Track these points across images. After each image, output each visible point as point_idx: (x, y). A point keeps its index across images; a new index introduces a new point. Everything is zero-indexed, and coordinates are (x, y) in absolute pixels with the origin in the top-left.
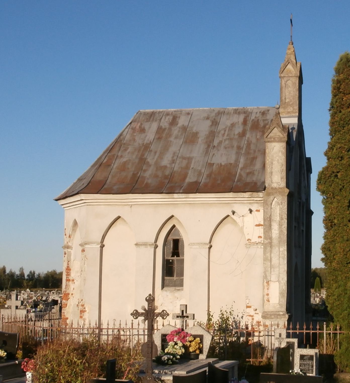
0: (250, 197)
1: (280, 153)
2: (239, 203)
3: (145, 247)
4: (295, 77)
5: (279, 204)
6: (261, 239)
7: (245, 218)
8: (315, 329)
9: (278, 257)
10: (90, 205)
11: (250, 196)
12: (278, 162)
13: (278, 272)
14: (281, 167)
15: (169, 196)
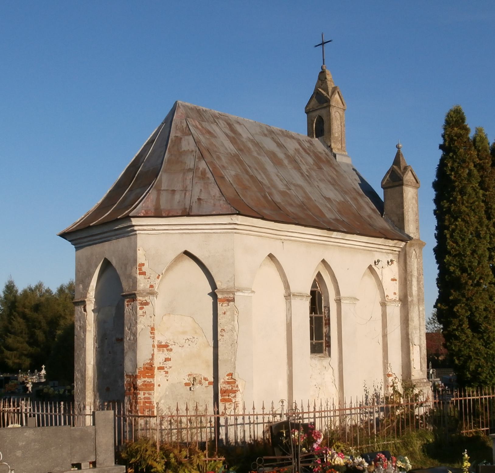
0: (391, 246)
2: (379, 252)
3: (301, 300)
4: (342, 110)
6: (396, 296)
7: (384, 270)
8: (461, 396)
10: (238, 233)
11: (393, 245)
12: (413, 210)
13: (419, 334)
14: (415, 216)
15: (328, 234)
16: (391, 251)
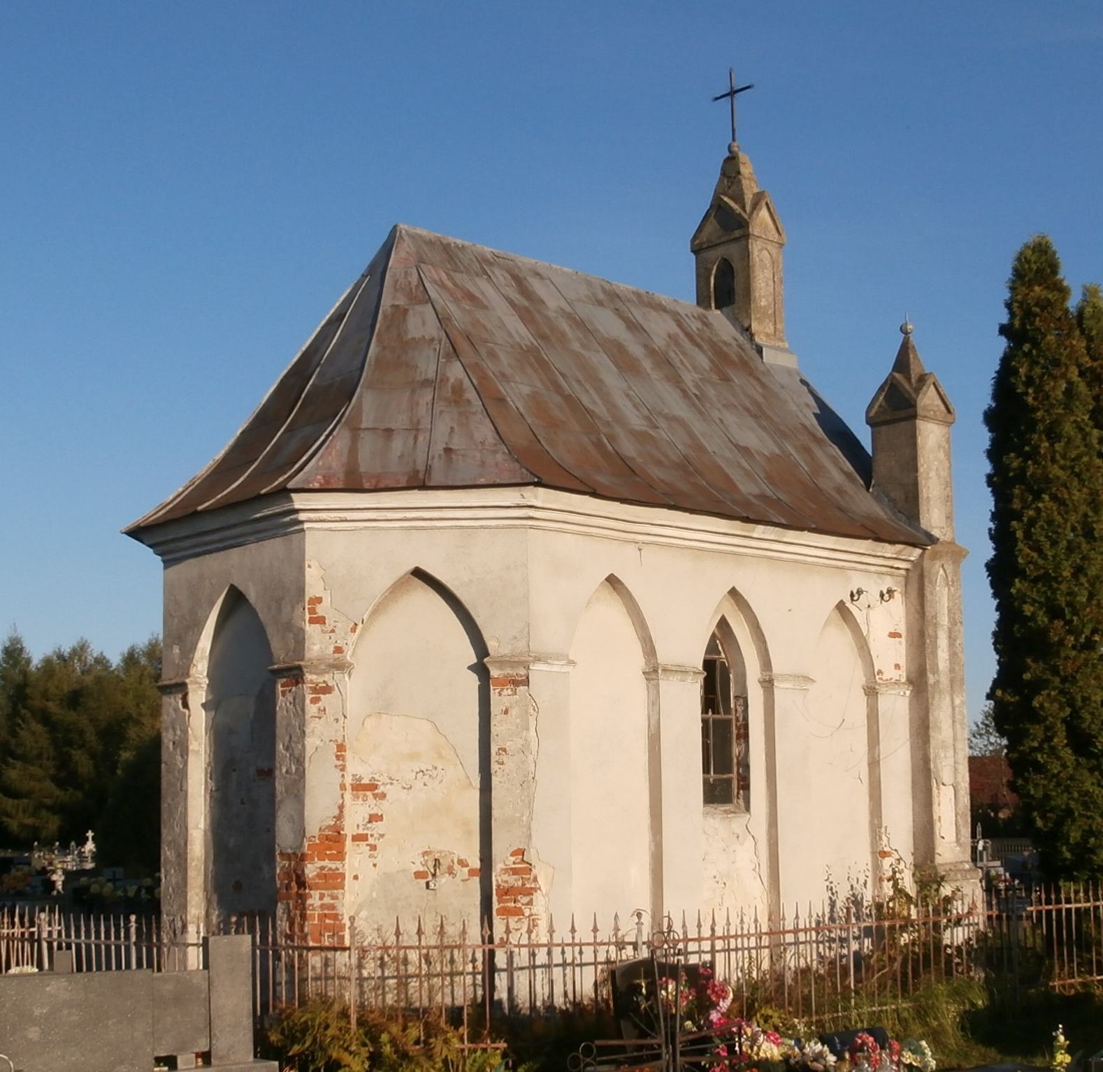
1: (942, 452)
2: (861, 571)
3: (681, 681)
5: (948, 584)
6: (900, 672)
7: (871, 612)
8: (1048, 902)
9: (951, 721)
10: (537, 528)
11: (894, 556)
15: (743, 530)
16: (889, 569)
